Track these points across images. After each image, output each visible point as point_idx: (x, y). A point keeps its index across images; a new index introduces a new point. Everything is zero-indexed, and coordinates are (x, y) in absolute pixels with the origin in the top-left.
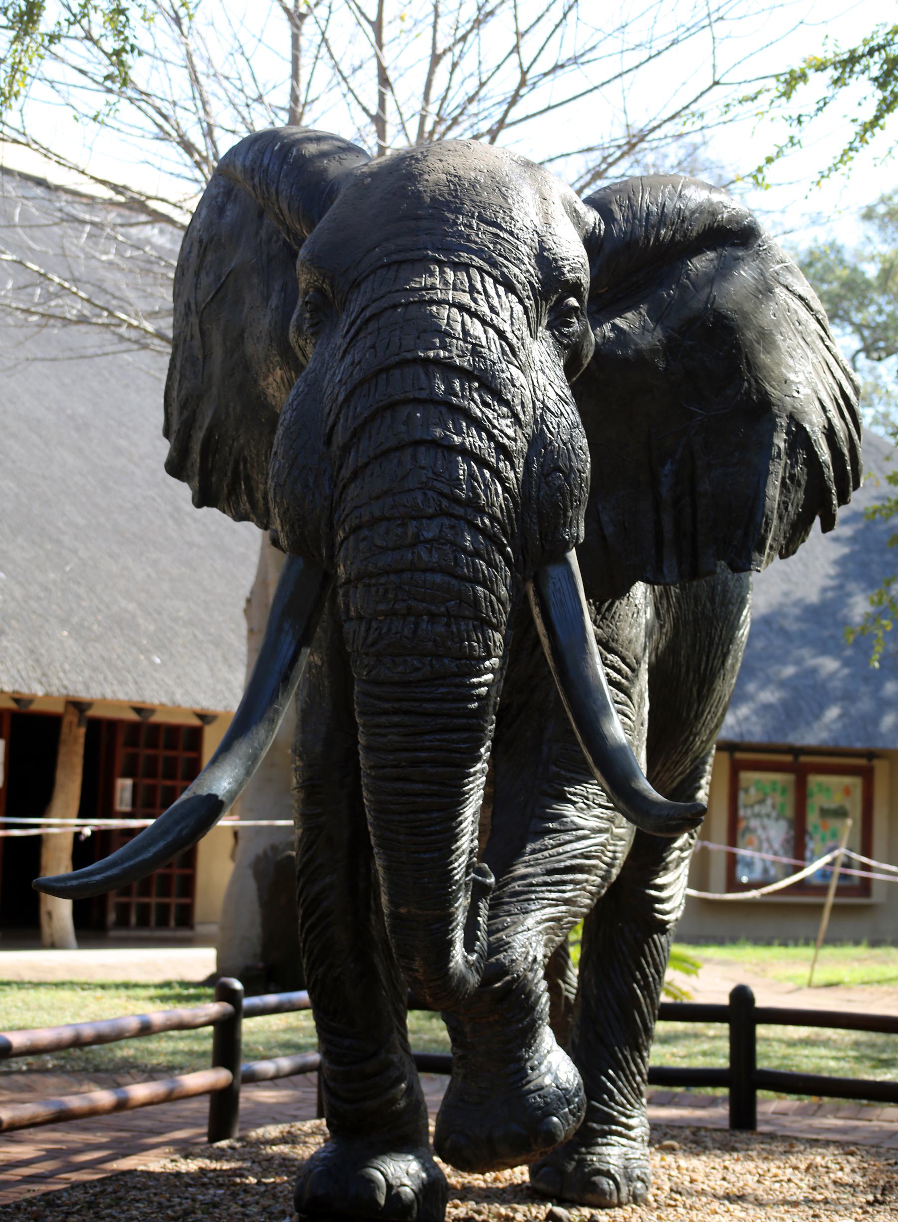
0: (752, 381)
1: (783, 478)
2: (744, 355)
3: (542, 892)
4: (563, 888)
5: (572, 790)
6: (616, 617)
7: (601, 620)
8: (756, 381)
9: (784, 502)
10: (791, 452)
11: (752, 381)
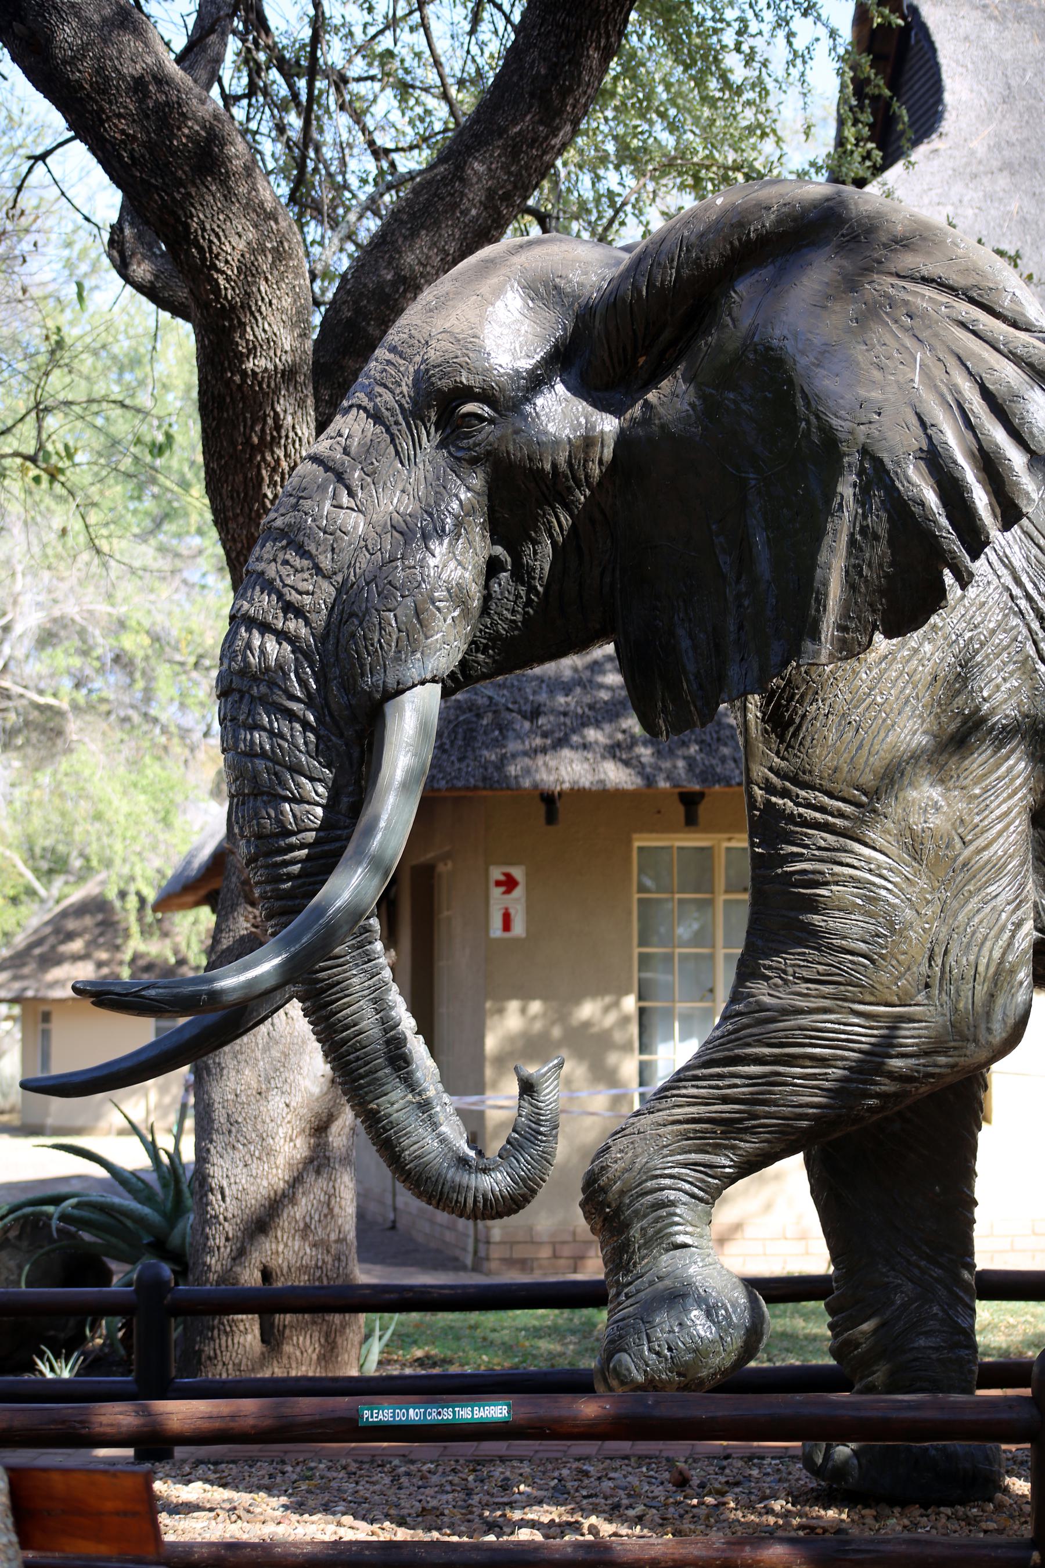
0: (813, 419)
1: (852, 535)
2: (798, 389)
3: (685, 1087)
4: (720, 1083)
5: (767, 962)
6: (807, 743)
7: (786, 749)
8: (818, 417)
9: (854, 566)
10: (863, 497)
11: (813, 419)
